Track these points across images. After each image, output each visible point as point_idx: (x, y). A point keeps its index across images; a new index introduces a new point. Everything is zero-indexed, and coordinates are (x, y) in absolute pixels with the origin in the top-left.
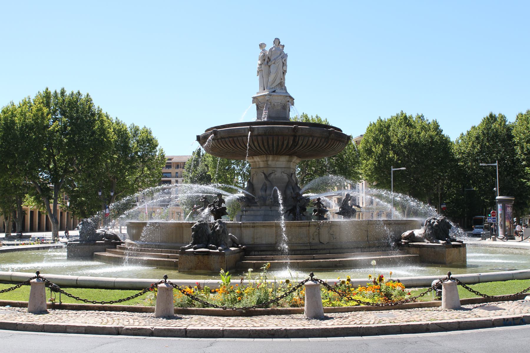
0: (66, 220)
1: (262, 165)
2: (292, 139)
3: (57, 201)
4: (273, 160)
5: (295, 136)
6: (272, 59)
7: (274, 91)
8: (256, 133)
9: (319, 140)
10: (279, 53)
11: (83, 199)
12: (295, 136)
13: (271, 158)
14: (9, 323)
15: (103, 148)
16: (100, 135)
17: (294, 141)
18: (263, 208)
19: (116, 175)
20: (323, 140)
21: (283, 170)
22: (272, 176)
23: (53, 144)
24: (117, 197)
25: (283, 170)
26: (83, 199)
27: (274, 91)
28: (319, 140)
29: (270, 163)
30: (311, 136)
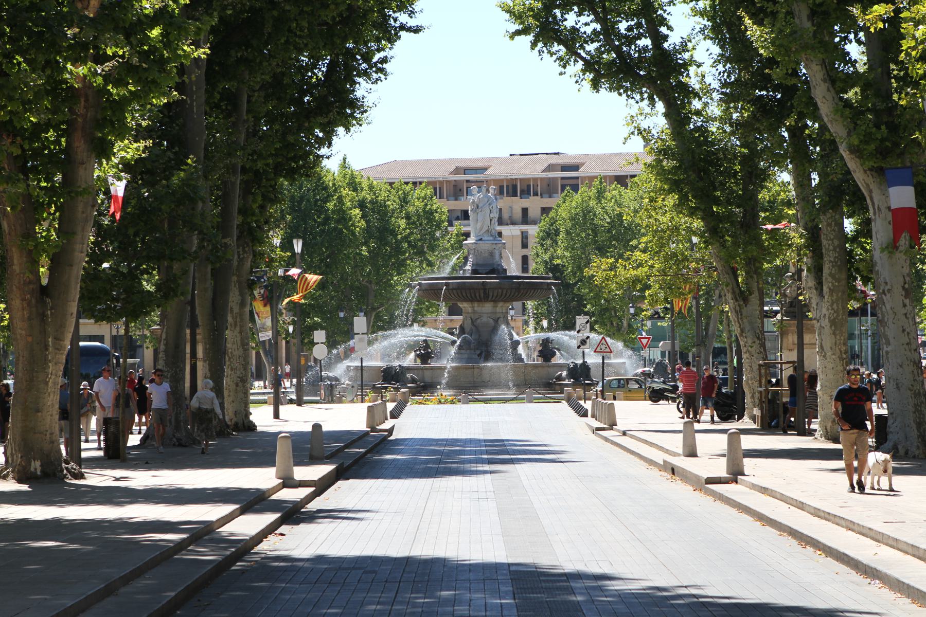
0: (284, 355)
1: (470, 310)
2: (482, 292)
3: (80, 441)
4: (478, 306)
5: (485, 289)
6: (480, 206)
7: (481, 240)
8: (451, 287)
9: (509, 291)
10: (486, 200)
11: (316, 319)
12: (485, 289)
13: (476, 304)
14: (47, 521)
15: (342, 246)
16: (338, 222)
17: (485, 293)
18: (468, 351)
19: (724, 90)
20: (514, 290)
21: (489, 315)
22: (479, 321)
23: (295, 162)
24: (377, 314)
25: (489, 315)
26: (316, 319)
27: (481, 240)
28: (509, 291)
29: (476, 309)
30: (500, 288)
